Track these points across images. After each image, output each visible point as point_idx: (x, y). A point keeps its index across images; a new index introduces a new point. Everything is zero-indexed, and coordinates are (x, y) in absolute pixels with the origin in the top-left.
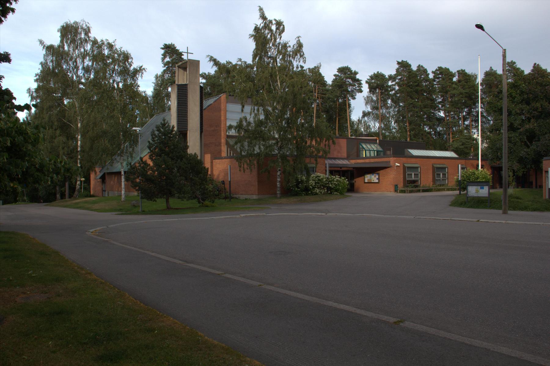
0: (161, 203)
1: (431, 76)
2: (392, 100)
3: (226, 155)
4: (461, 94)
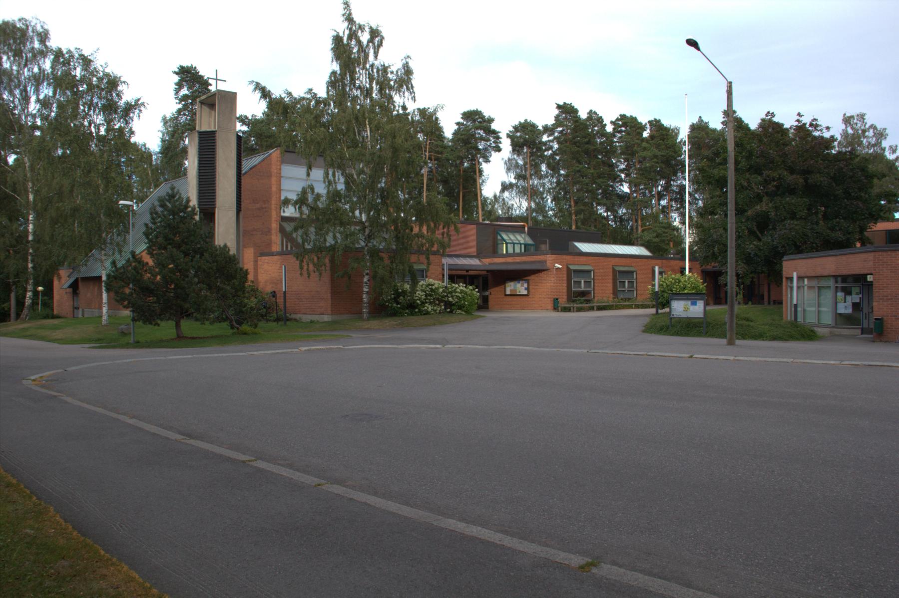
0: (167, 328)
1: (609, 128)
2: (549, 166)
3: (279, 249)
4: (655, 156)
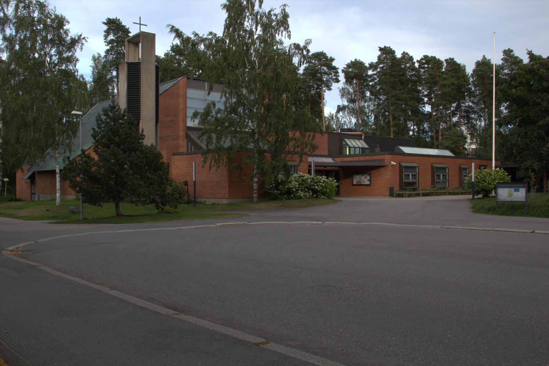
0: (108, 208)
2: (372, 94)
4: (453, 84)
